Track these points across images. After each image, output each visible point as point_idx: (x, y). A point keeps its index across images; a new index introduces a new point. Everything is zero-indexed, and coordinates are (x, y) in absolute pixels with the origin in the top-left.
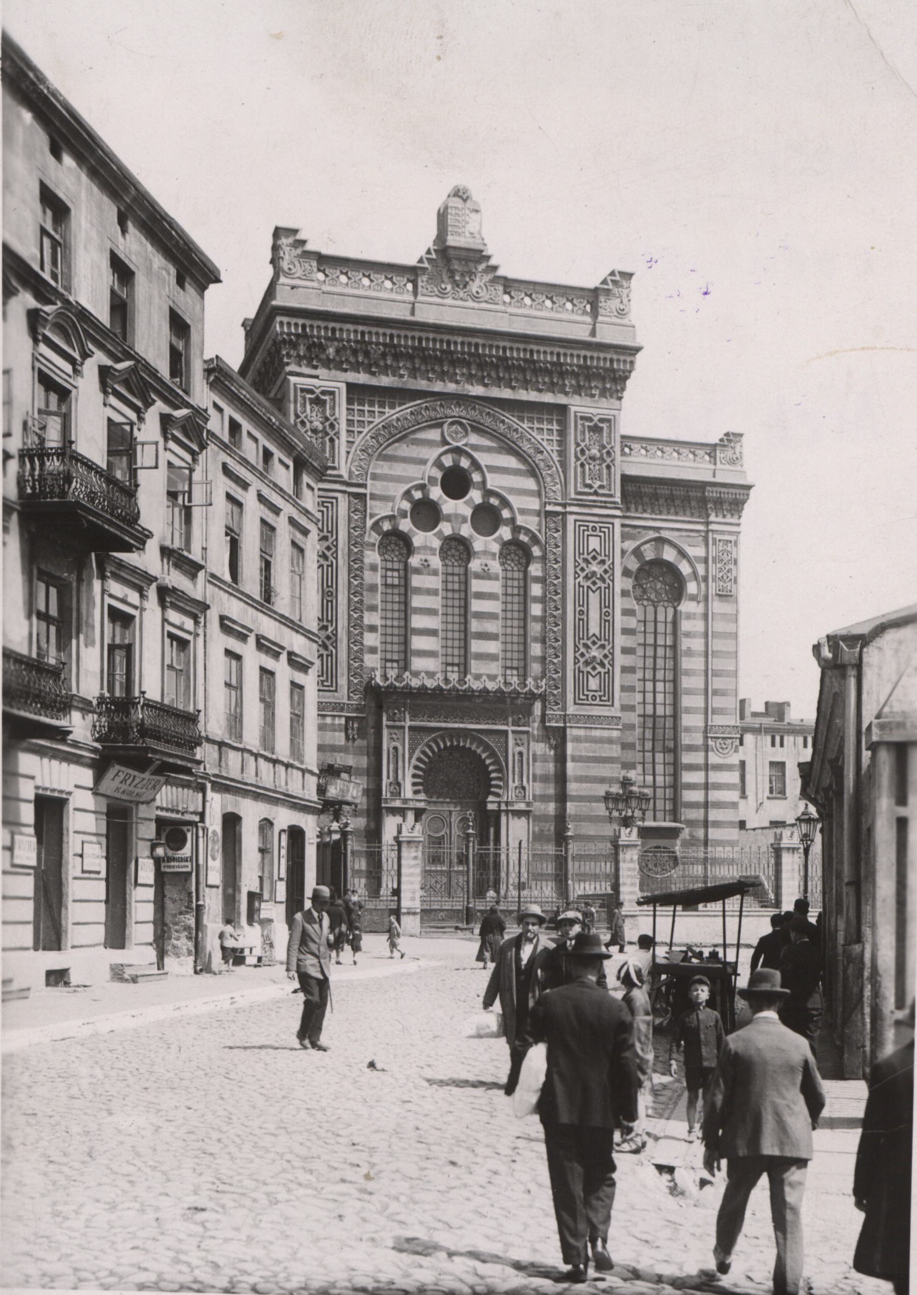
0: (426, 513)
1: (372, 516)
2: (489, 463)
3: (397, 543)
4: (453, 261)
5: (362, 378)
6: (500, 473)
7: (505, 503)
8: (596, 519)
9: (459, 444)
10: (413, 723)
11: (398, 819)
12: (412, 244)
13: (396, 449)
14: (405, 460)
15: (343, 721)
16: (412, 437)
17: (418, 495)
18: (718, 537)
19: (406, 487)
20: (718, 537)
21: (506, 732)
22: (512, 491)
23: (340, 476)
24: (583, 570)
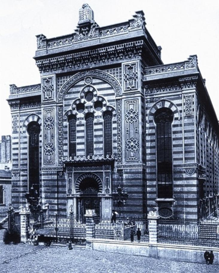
0: (80, 107)
1: (65, 111)
2: (98, 88)
3: (72, 118)
4: (86, 27)
5: (60, 71)
6: (101, 90)
7: (104, 99)
8: (132, 98)
9: (89, 84)
10: (75, 171)
11: (72, 200)
12: (71, 29)
13: (72, 90)
14: (74, 93)
15: (56, 172)
16: (76, 85)
17: (78, 102)
18: (185, 95)
19: (74, 101)
20: (185, 95)
21: (102, 172)
22: (105, 95)
23: (55, 102)
24: (128, 116)
